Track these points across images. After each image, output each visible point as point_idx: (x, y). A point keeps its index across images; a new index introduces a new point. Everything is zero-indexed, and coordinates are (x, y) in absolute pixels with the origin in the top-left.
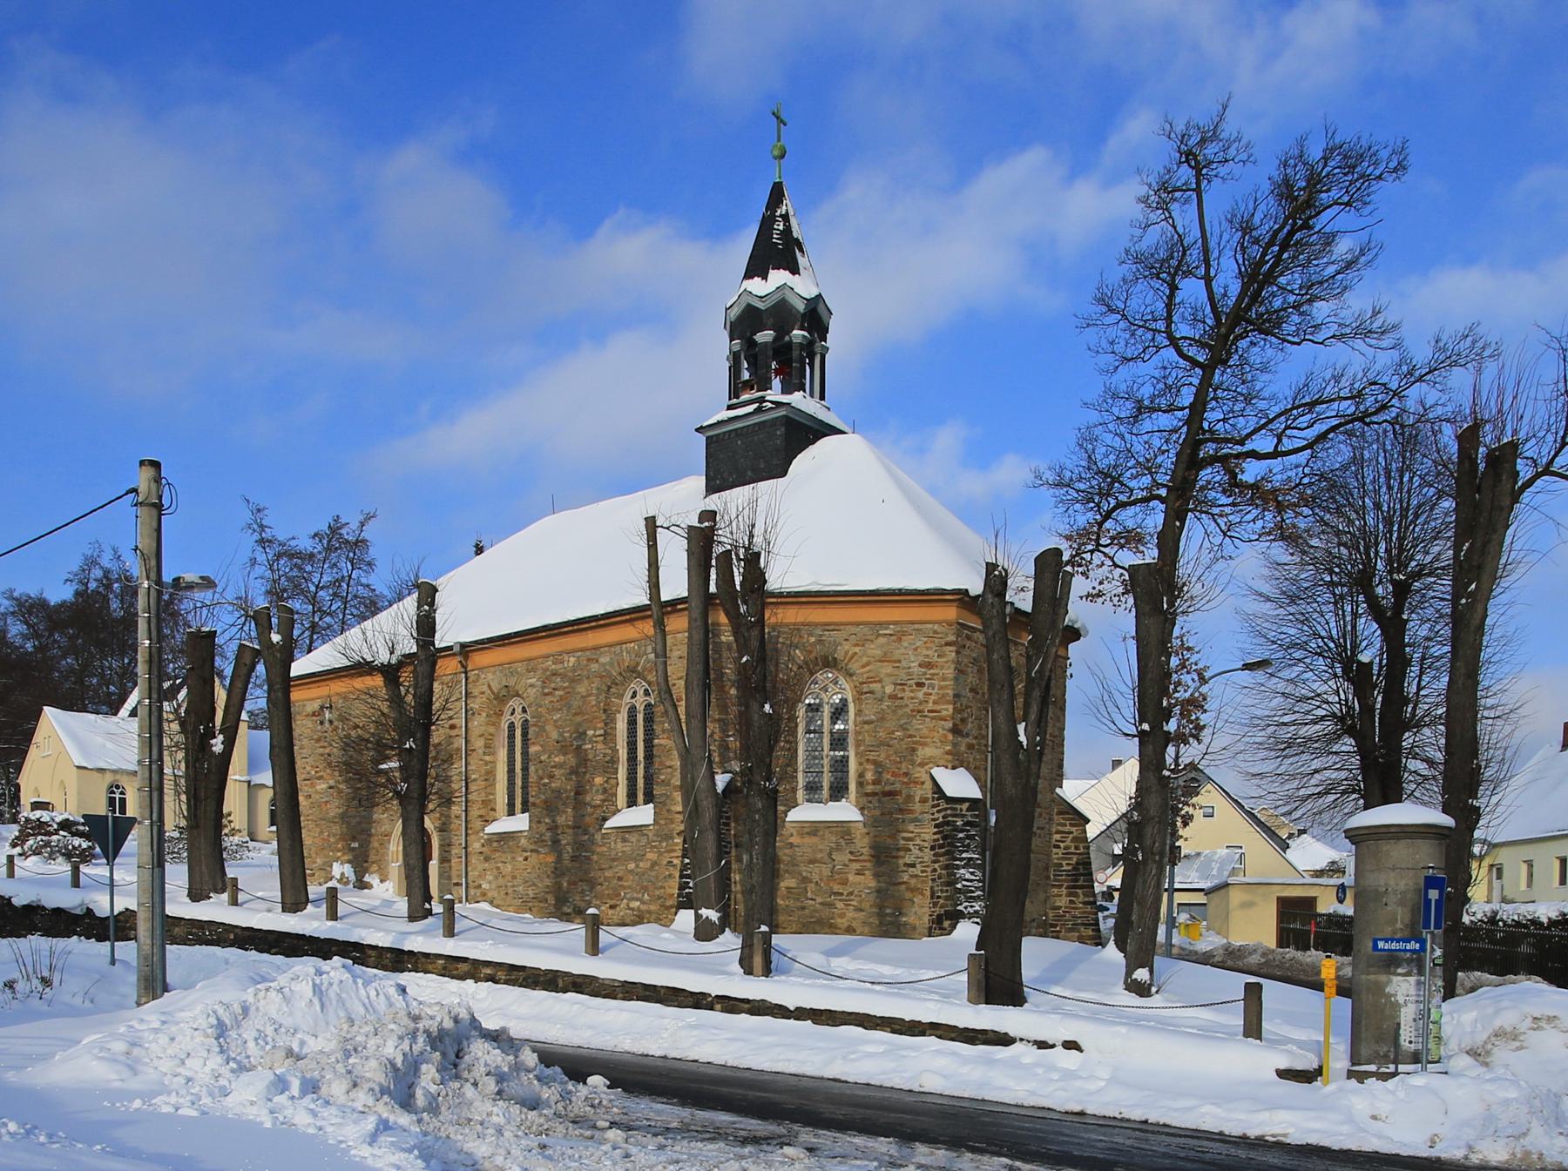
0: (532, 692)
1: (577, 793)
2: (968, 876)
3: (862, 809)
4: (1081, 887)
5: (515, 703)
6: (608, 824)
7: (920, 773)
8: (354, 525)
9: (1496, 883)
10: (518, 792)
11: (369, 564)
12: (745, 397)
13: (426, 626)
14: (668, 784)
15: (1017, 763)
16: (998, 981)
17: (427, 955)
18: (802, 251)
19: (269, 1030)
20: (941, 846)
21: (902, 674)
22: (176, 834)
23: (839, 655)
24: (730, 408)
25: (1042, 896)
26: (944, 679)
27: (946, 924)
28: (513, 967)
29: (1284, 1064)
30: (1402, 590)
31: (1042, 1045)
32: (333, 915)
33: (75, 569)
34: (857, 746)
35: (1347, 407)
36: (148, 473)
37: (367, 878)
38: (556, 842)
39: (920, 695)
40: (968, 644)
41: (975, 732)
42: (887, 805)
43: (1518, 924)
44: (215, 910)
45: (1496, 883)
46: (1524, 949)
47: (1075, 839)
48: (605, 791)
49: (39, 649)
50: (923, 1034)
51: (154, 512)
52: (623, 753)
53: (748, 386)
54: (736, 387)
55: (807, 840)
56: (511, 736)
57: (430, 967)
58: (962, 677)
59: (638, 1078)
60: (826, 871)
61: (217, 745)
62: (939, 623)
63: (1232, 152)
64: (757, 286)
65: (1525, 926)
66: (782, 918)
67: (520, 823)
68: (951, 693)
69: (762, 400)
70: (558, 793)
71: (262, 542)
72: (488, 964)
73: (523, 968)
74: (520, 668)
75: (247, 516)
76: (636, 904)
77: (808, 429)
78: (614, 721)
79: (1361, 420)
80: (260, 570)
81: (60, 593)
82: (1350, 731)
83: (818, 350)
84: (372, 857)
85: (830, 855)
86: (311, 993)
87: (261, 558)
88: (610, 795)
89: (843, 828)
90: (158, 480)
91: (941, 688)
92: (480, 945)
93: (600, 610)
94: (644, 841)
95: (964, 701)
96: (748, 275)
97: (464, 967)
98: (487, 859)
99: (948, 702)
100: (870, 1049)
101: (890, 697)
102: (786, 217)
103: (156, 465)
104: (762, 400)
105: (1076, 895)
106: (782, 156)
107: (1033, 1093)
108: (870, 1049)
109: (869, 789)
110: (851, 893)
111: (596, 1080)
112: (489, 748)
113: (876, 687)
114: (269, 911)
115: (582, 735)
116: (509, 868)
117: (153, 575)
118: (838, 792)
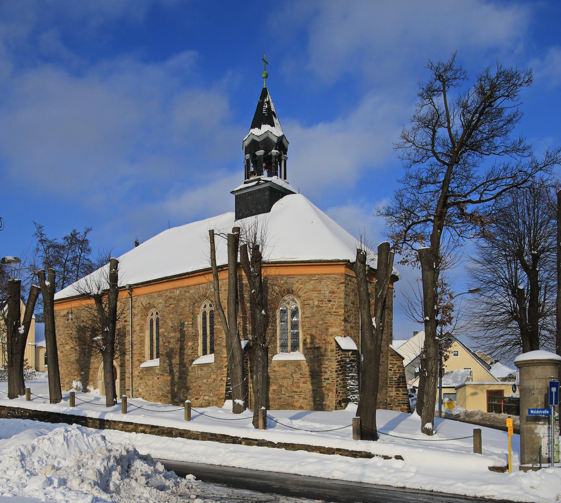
0: (160, 306)
1: (181, 349)
2: (352, 383)
3: (305, 355)
4: (401, 387)
5: (153, 310)
6: (194, 363)
7: (330, 339)
8: (82, 234)
11: (89, 250)
12: (252, 178)
13: (114, 278)
14: (220, 345)
16: (366, 430)
17: (115, 422)
19: (44, 457)
20: (340, 371)
21: (322, 297)
23: (294, 288)
24: (245, 183)
25: (384, 391)
26: (340, 298)
27: (343, 404)
28: (153, 427)
29: (492, 464)
30: (536, 258)
31: (386, 457)
32: (73, 404)
34: (303, 327)
35: (510, 181)
37: (88, 388)
38: (171, 371)
39: (330, 305)
41: (354, 321)
42: (315, 355)
44: (20, 403)
47: (398, 367)
48: (193, 348)
50: (333, 453)
52: (201, 332)
53: (253, 174)
54: (247, 176)
56: (152, 325)
57: (116, 427)
58: (348, 297)
60: (290, 382)
61: (21, 330)
62: (337, 274)
63: (458, 75)
64: (256, 132)
66: (271, 403)
67: (156, 362)
68: (343, 304)
69: (259, 180)
70: (172, 350)
71: (41, 241)
73: (157, 427)
75: (35, 230)
76: (207, 398)
78: (196, 318)
79: (516, 186)
80: (41, 253)
82: (516, 318)
83: (283, 158)
84: (90, 378)
85: (292, 375)
86: (62, 440)
87: (41, 248)
88: (195, 350)
89: (297, 364)
91: (339, 302)
92: (138, 417)
93: (190, 270)
94: (210, 370)
95: (349, 308)
96: (253, 127)
97: (131, 427)
98: (141, 379)
99: (342, 308)
100: (311, 460)
101: (317, 306)
102: (268, 103)
104: (259, 180)
105: (399, 391)
107: (382, 479)
109: (309, 346)
110: (301, 392)
111: (190, 477)
112: (142, 330)
113: (310, 302)
114: (44, 403)
115: (182, 324)
118: (295, 347)
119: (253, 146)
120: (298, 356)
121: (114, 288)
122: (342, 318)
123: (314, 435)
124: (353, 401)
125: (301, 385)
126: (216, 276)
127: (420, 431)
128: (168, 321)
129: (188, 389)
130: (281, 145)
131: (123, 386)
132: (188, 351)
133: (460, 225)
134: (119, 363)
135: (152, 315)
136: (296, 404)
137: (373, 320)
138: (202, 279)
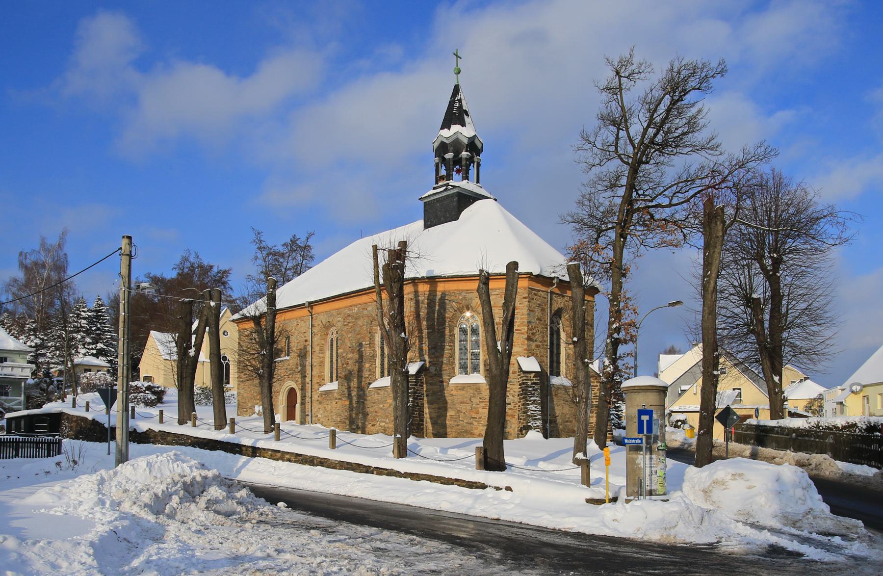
0: (339, 324)
2: (534, 409)
5: (333, 329)
6: (371, 386)
8: (303, 239)
9: (867, 406)
10: (335, 371)
11: (311, 257)
12: (440, 184)
15: (497, 360)
16: (492, 460)
17: (264, 449)
18: (467, 115)
19: (124, 482)
22: (199, 392)
24: (434, 189)
27: (524, 432)
28: (298, 455)
29: (589, 497)
30: (777, 263)
31: (498, 489)
32: (233, 431)
33: (178, 263)
35: (706, 182)
36: (126, 241)
38: (350, 395)
40: (535, 297)
41: (540, 339)
43: (828, 428)
44: (187, 430)
45: (867, 406)
46: (829, 440)
49: (163, 300)
50: (452, 484)
51: (128, 257)
53: (442, 178)
54: (438, 178)
55: (460, 392)
56: (332, 345)
58: (532, 314)
59: (299, 502)
61: (192, 352)
63: (643, 68)
64: (446, 133)
65: (832, 429)
67: (334, 386)
69: (447, 185)
70: (350, 373)
71: (260, 248)
72: (288, 453)
73: (301, 455)
74: (335, 313)
75: (253, 237)
77: (470, 197)
78: (374, 337)
79: (714, 187)
80: (260, 262)
81: (171, 274)
82: (752, 332)
86: (145, 466)
87: (260, 255)
88: (372, 373)
89: (476, 387)
90: (130, 244)
95: (533, 325)
96: (442, 128)
97: (279, 455)
98: (320, 403)
100: (428, 491)
102: (460, 101)
103: (130, 238)
104: (447, 185)
106: (459, 73)
107: (483, 510)
108: (428, 491)
111: (281, 504)
112: (322, 351)
114: (209, 429)
115: (361, 345)
116: (330, 407)
117: (127, 285)
118: (476, 369)
119: (442, 149)
120: (479, 378)
121: (273, 312)
122: (525, 336)
123: (442, 465)
124: (535, 428)
125: (481, 410)
126: (379, 294)
127: (571, 464)
128: (346, 341)
129: (366, 415)
130: (473, 147)
131: (303, 411)
132: (366, 374)
133: (639, 233)
134: (300, 386)
135: (333, 334)
136: (475, 431)
137: (499, 344)
138: (364, 299)
